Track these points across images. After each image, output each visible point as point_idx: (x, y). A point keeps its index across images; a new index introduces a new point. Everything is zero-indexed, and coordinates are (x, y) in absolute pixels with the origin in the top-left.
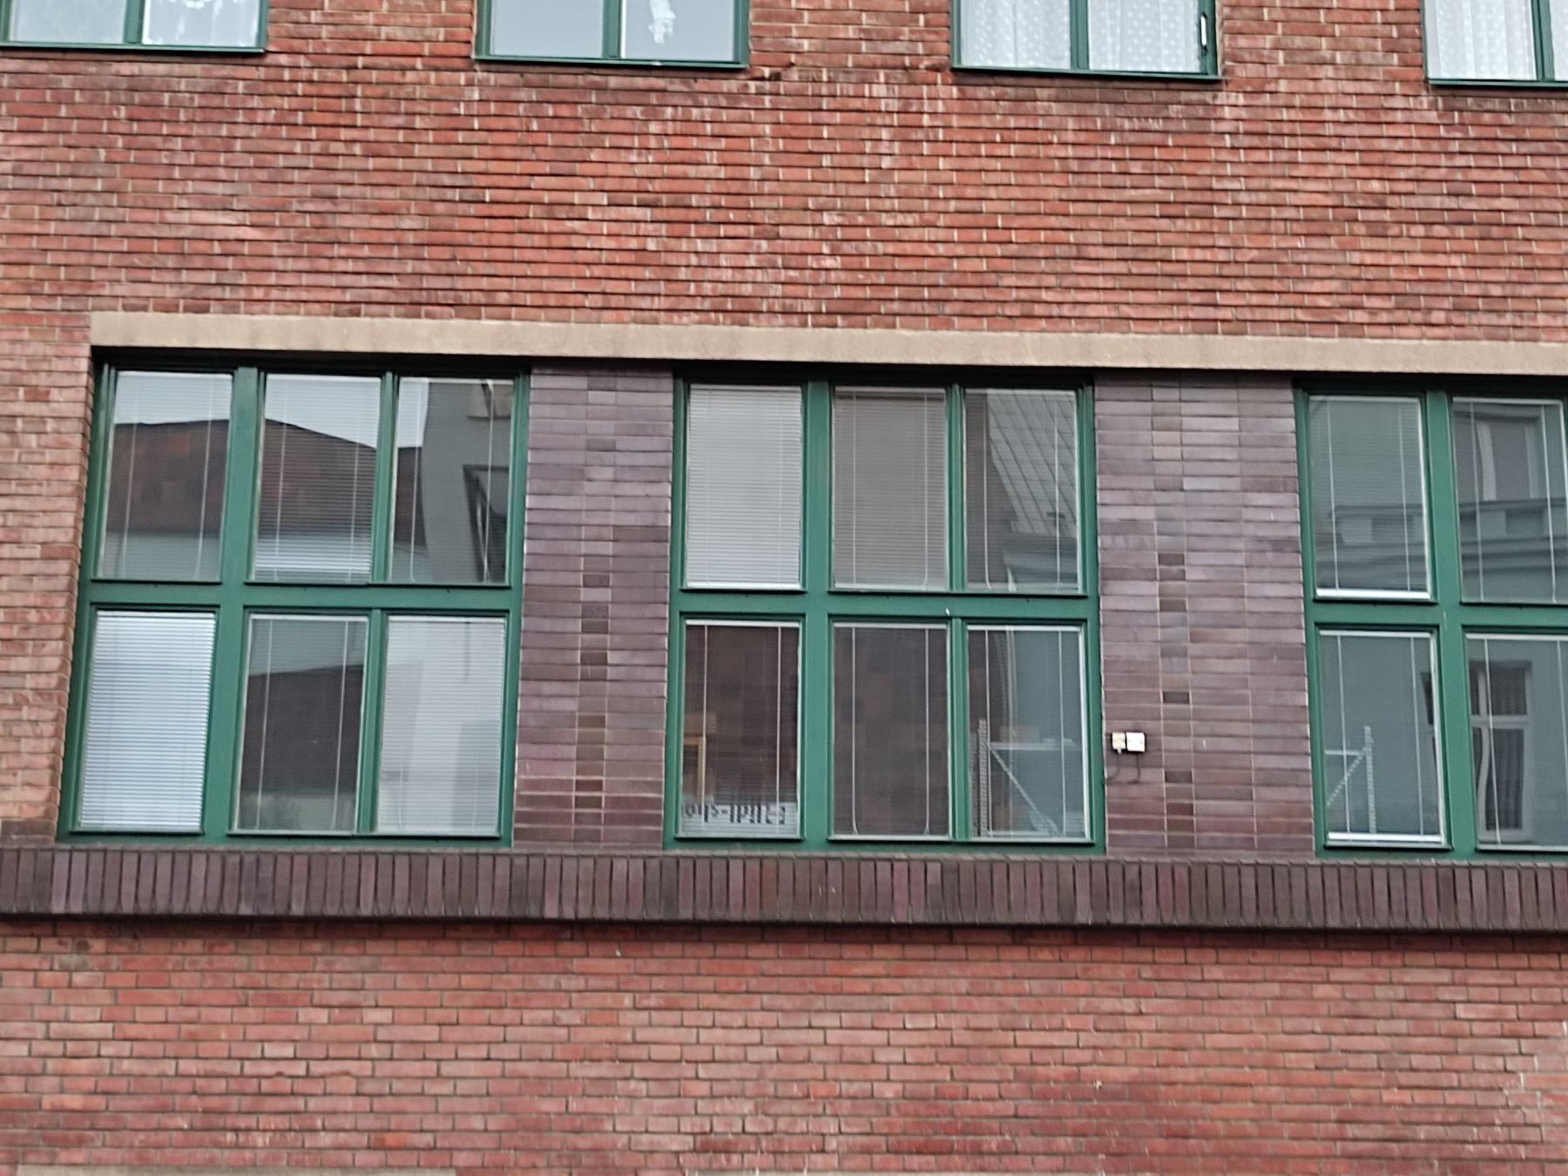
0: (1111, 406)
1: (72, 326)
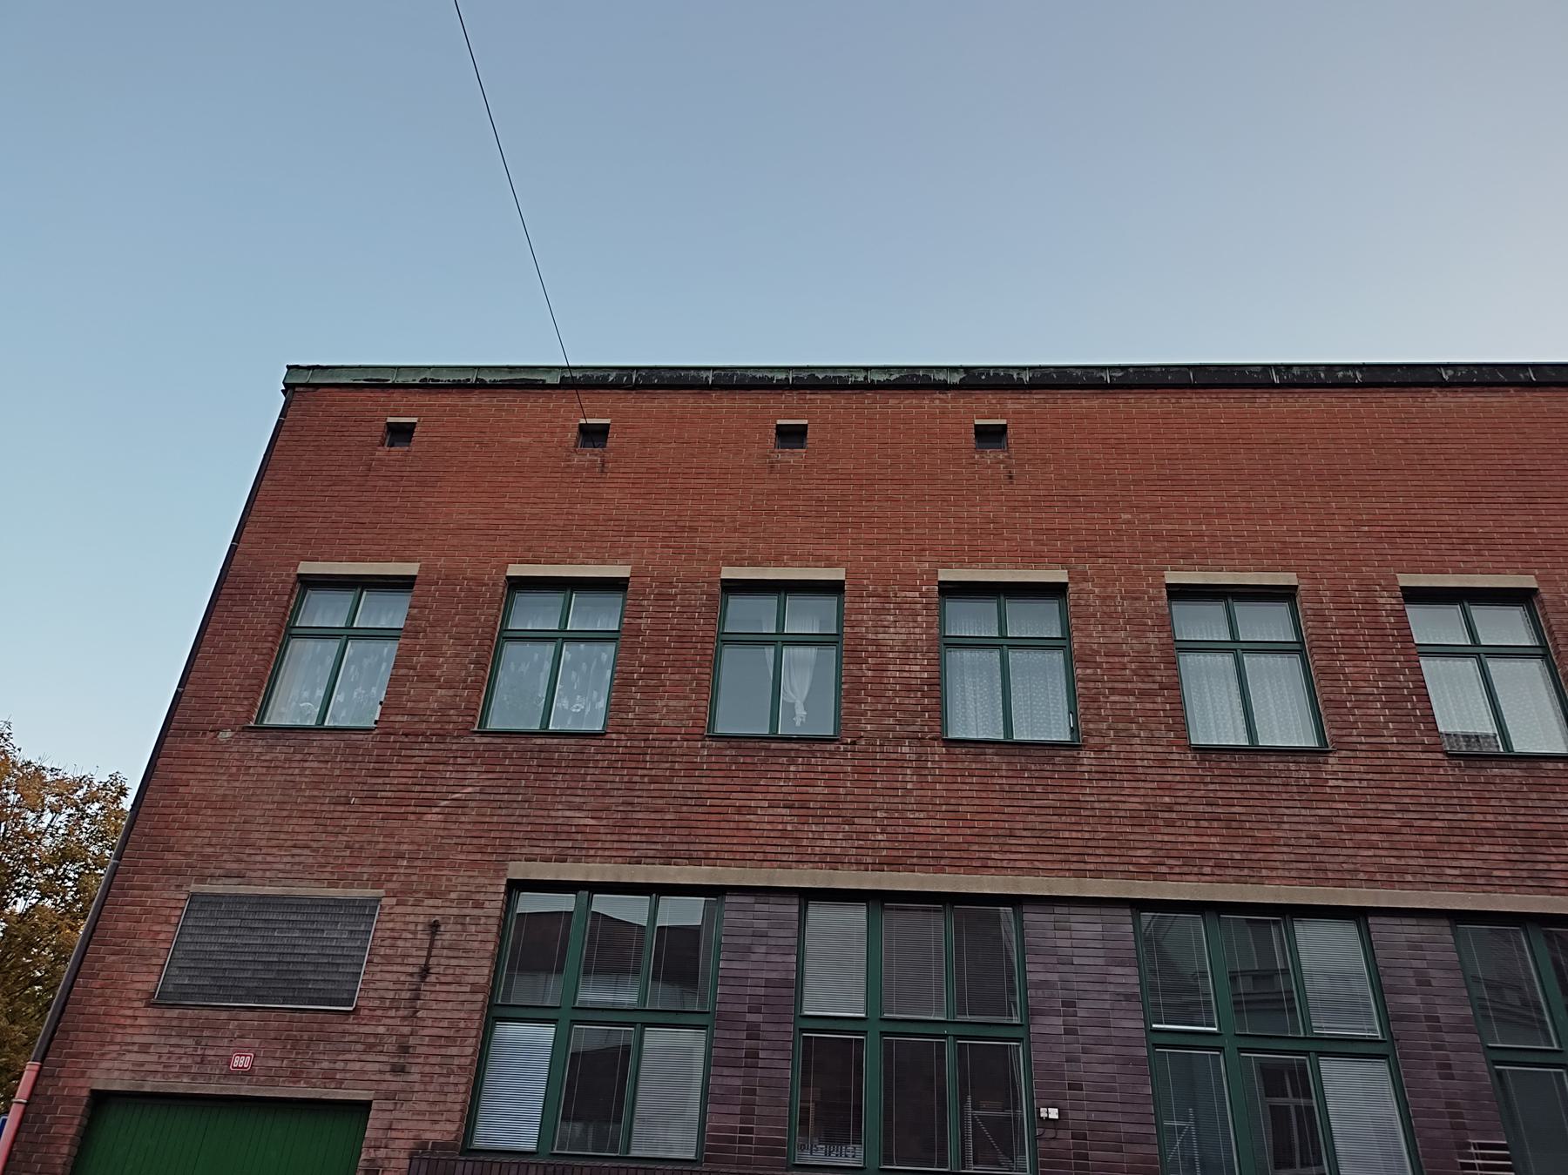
0: (1031, 916)
1: (500, 869)
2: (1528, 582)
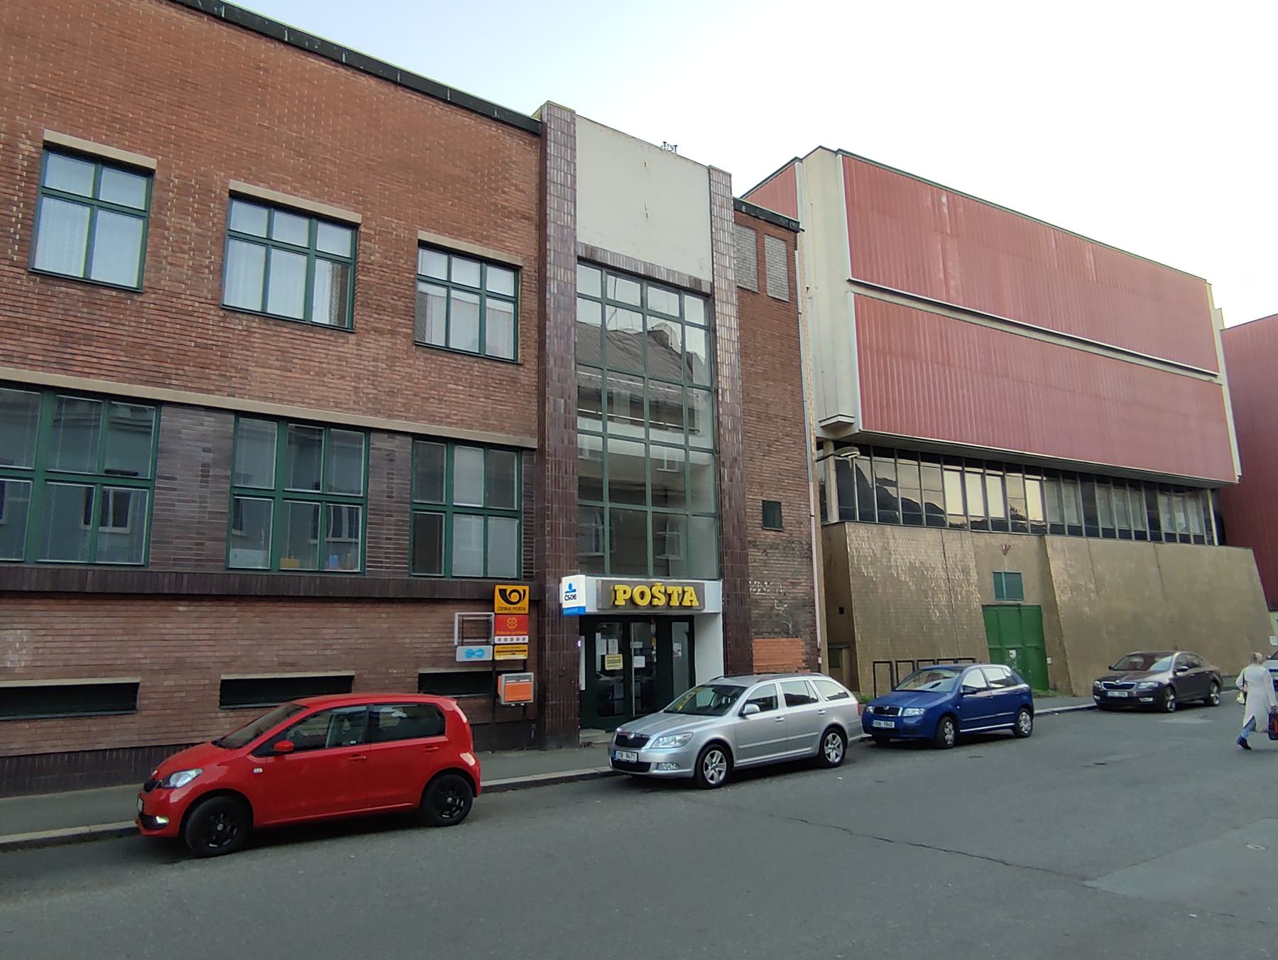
2: (150, 163)
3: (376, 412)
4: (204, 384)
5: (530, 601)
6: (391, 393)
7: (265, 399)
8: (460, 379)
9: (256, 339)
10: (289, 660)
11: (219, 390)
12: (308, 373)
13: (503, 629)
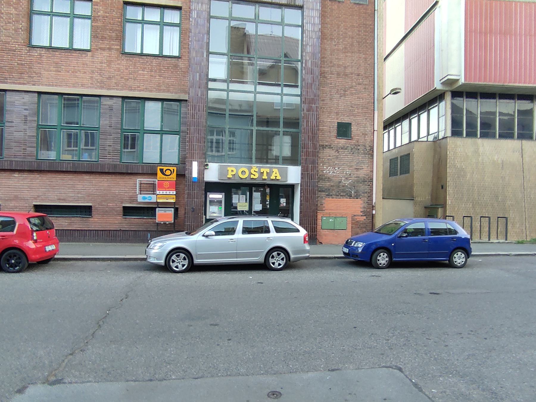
3: (102, 88)
4: (21, 81)
5: (177, 175)
6: (109, 78)
7: (49, 85)
8: (145, 68)
9: (44, 59)
10: (62, 198)
11: (28, 83)
12: (68, 72)
13: (161, 187)
